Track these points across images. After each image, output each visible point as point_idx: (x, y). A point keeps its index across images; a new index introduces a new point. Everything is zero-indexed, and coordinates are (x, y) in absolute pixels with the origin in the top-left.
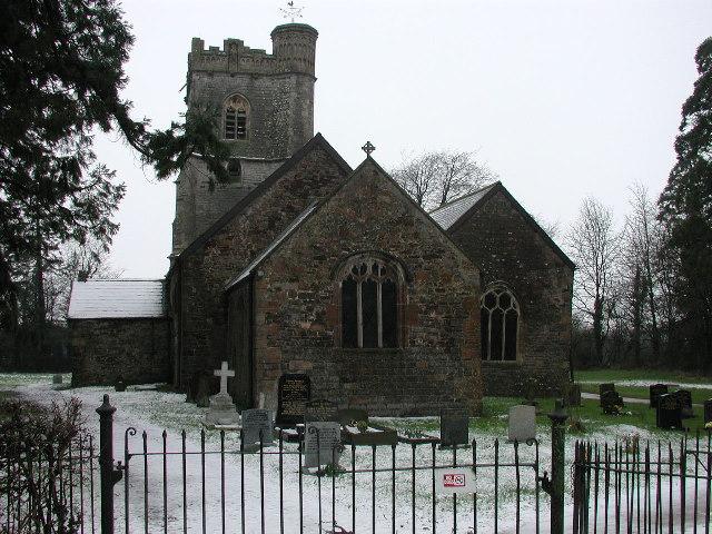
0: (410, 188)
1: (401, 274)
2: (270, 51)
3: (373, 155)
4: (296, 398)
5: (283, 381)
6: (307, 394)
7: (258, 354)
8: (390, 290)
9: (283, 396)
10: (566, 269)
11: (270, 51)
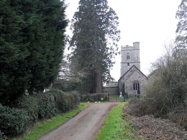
8: (139, 84)
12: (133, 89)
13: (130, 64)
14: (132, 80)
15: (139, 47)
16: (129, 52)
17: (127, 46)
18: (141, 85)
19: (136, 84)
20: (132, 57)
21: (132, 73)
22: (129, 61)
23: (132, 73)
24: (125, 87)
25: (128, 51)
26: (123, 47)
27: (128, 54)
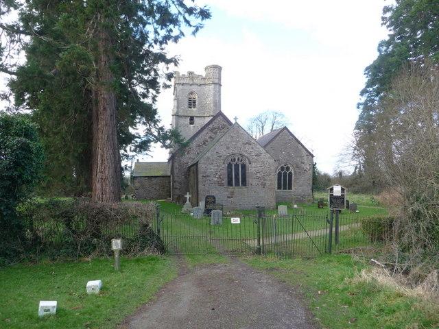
0: (250, 132)
1: (247, 161)
2: (333, 149)
3: (238, 121)
4: (211, 203)
5: (207, 198)
6: (214, 202)
7: (199, 189)
8: (244, 167)
9: (207, 203)
10: (310, 157)
11: (333, 149)
12: (225, 181)
13: (196, 120)
14: (224, 152)
15: (220, 79)
16: (194, 88)
17: (190, 73)
18: (252, 169)
19: (237, 166)
20: (199, 104)
21: (213, 136)
22: (194, 111)
23: (213, 136)
24: (200, 176)
25: (193, 87)
26: (181, 75)
27: (192, 93)
